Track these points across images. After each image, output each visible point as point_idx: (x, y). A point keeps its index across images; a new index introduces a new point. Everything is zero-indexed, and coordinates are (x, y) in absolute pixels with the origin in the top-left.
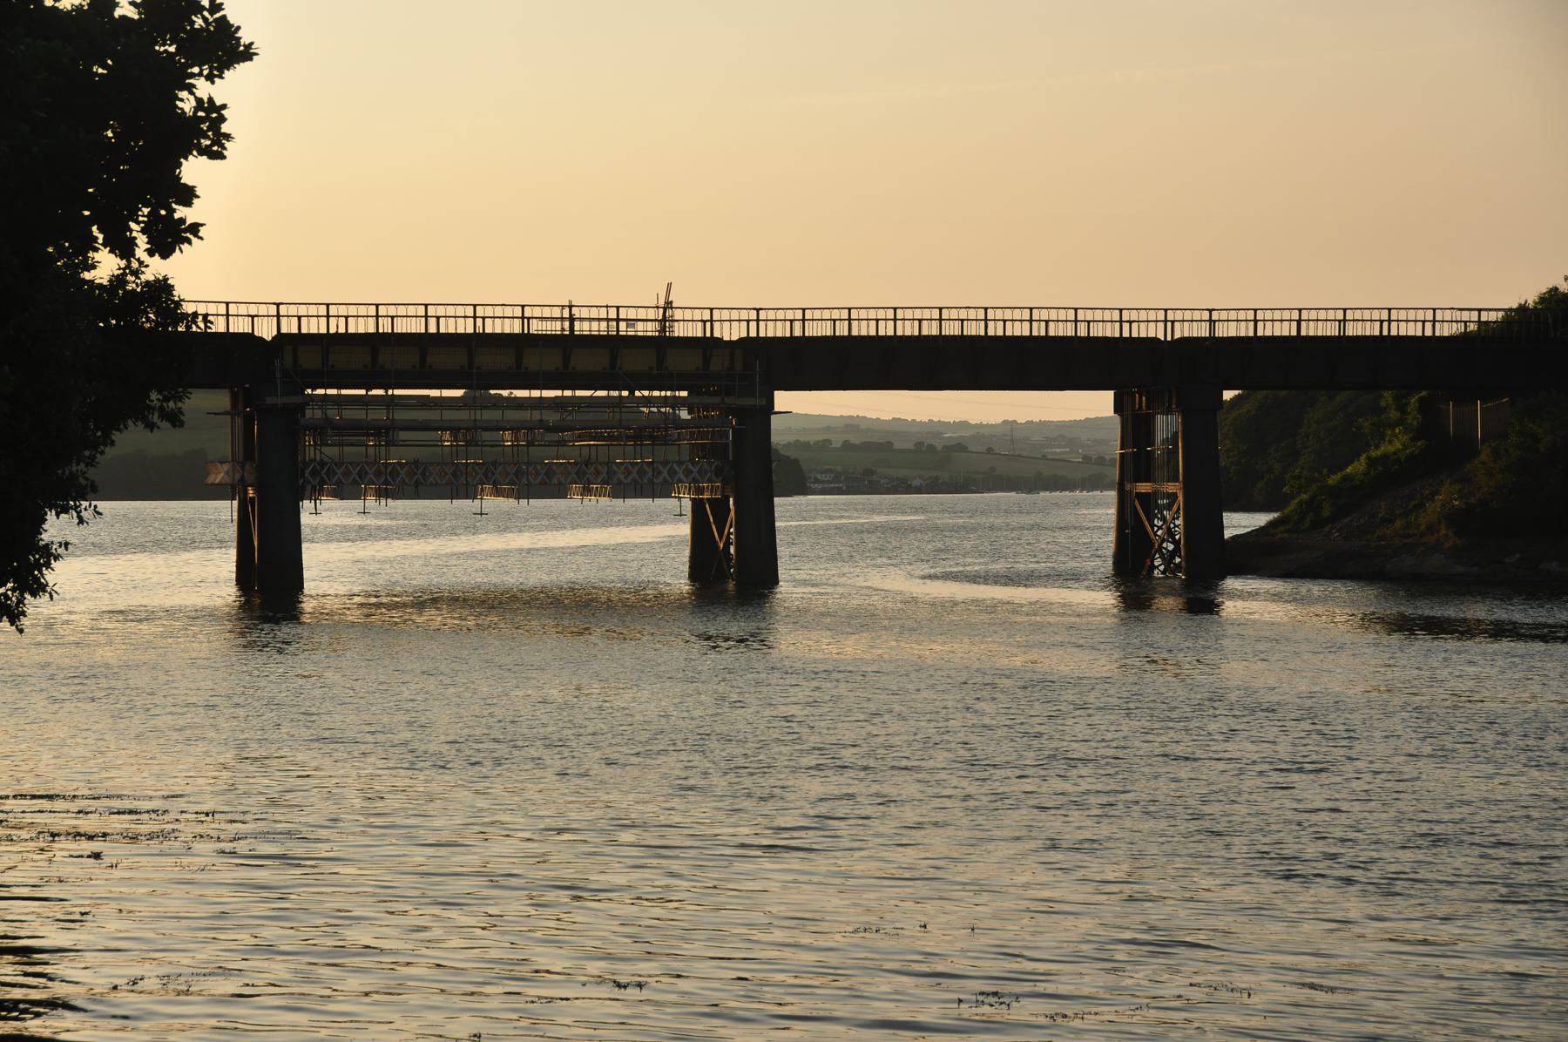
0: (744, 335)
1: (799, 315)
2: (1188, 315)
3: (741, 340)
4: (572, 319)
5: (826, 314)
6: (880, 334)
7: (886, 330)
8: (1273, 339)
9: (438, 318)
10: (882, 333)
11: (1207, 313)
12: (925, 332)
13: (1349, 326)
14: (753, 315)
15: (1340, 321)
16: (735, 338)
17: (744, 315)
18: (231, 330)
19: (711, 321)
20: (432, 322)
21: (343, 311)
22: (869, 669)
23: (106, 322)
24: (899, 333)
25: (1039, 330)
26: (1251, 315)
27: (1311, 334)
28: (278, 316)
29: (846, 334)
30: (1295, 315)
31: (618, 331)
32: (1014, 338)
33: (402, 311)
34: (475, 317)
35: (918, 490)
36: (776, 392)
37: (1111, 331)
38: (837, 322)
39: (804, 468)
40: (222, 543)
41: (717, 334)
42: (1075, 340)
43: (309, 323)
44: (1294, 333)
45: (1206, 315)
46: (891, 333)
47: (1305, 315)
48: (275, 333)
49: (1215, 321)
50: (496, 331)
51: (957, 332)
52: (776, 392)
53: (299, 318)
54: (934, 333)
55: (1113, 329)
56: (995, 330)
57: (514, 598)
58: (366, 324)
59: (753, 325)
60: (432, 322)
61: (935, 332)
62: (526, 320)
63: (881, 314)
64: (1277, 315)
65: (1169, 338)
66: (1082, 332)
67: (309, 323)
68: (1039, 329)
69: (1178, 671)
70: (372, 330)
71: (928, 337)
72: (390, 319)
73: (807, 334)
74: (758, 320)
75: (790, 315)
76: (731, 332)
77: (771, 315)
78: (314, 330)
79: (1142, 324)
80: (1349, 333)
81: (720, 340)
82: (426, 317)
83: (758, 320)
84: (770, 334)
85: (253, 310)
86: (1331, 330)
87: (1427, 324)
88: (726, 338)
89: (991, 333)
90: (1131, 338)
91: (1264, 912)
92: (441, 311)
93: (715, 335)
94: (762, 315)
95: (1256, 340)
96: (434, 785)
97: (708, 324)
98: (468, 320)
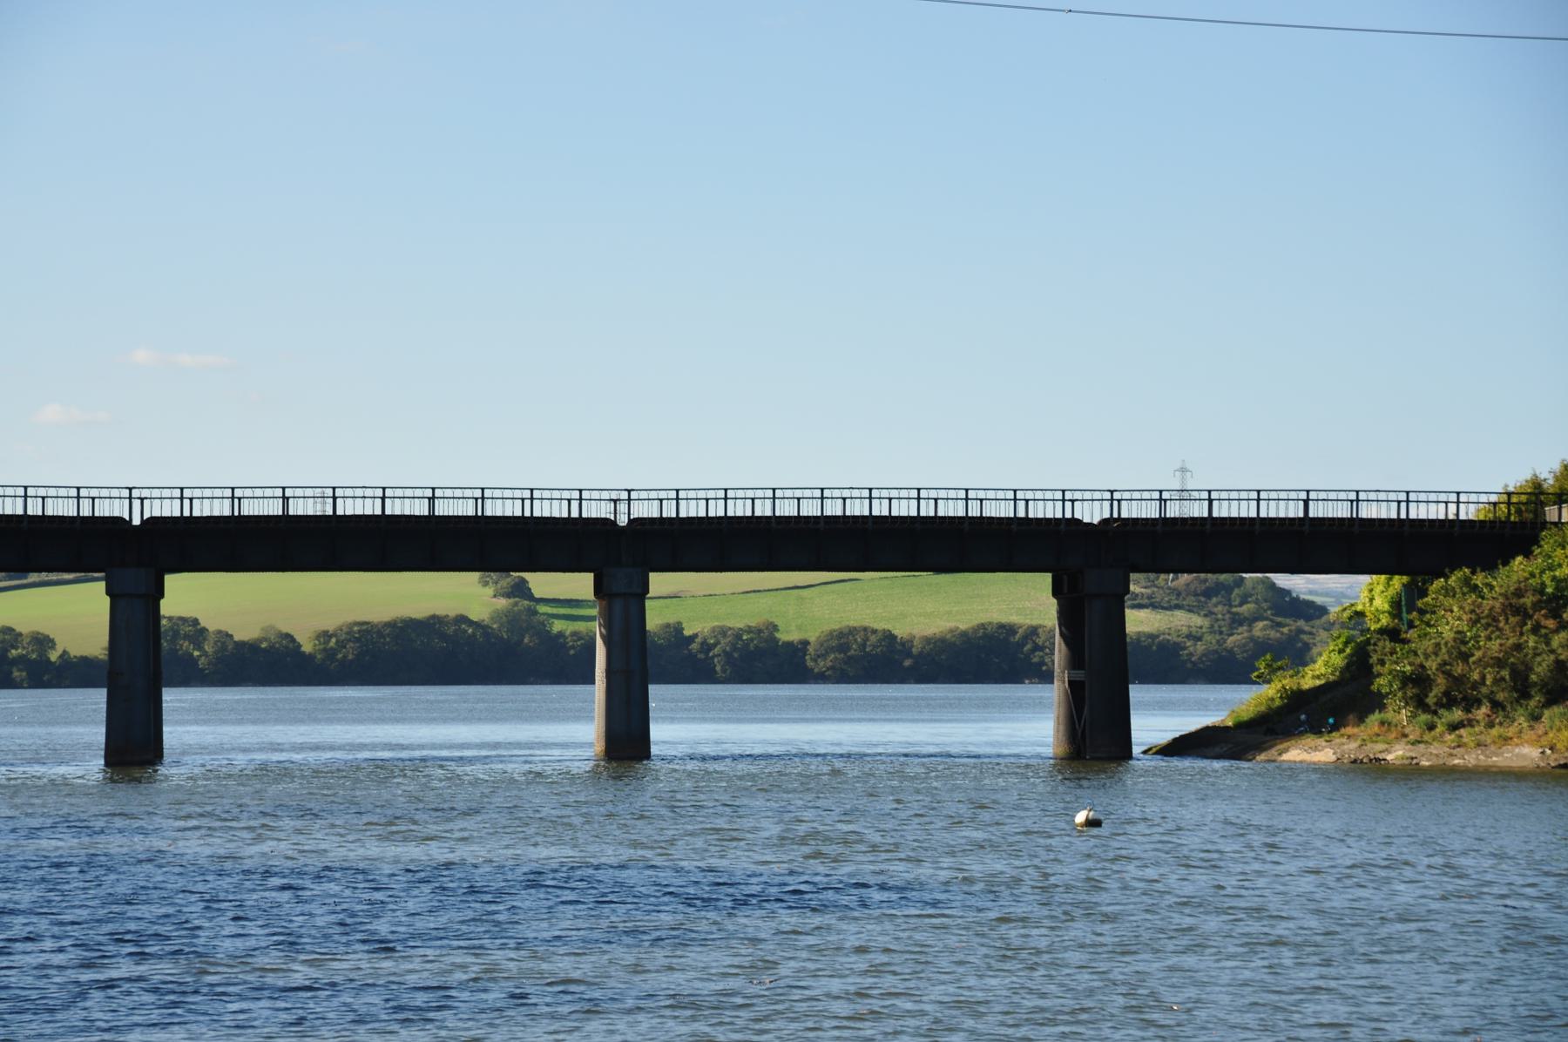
0: (1107, 515)
2: (208, 493)
3: (1104, 522)
5: (653, 495)
6: (874, 513)
7: (717, 510)
8: (1183, 521)
9: (142, 499)
10: (758, 513)
11: (626, 493)
13: (1363, 505)
15: (429, 498)
18: (97, 514)
20: (1021, 505)
21: (933, 494)
22: (1228, 849)
24: (730, 513)
25: (927, 510)
26: (379, 493)
29: (75, 514)
30: (1303, 495)
33: (52, 492)
36: (652, 575)
37: (1003, 510)
38: (96, 500)
40: (94, 722)
42: (78, 520)
44: (1301, 515)
45: (1108, 495)
46: (721, 513)
47: (238, 493)
48: (626, 521)
53: (569, 501)
55: (1201, 508)
56: (880, 509)
59: (575, 504)
60: (1021, 505)
62: (236, 501)
63: (711, 494)
64: (1234, 495)
65: (236, 514)
66: (86, 511)
70: (961, 513)
71: (689, 519)
72: (796, 501)
73: (970, 515)
74: (1408, 501)
76: (1092, 513)
79: (1243, 503)
80: (1364, 514)
81: (1079, 522)
82: (1015, 500)
85: (798, 494)
86: (1295, 511)
87: (1449, 505)
89: (875, 513)
90: (1027, 519)
91: (820, 973)
93: (1076, 516)
95: (1164, 521)
96: (630, 959)
97: (480, 501)
98: (516, 501)
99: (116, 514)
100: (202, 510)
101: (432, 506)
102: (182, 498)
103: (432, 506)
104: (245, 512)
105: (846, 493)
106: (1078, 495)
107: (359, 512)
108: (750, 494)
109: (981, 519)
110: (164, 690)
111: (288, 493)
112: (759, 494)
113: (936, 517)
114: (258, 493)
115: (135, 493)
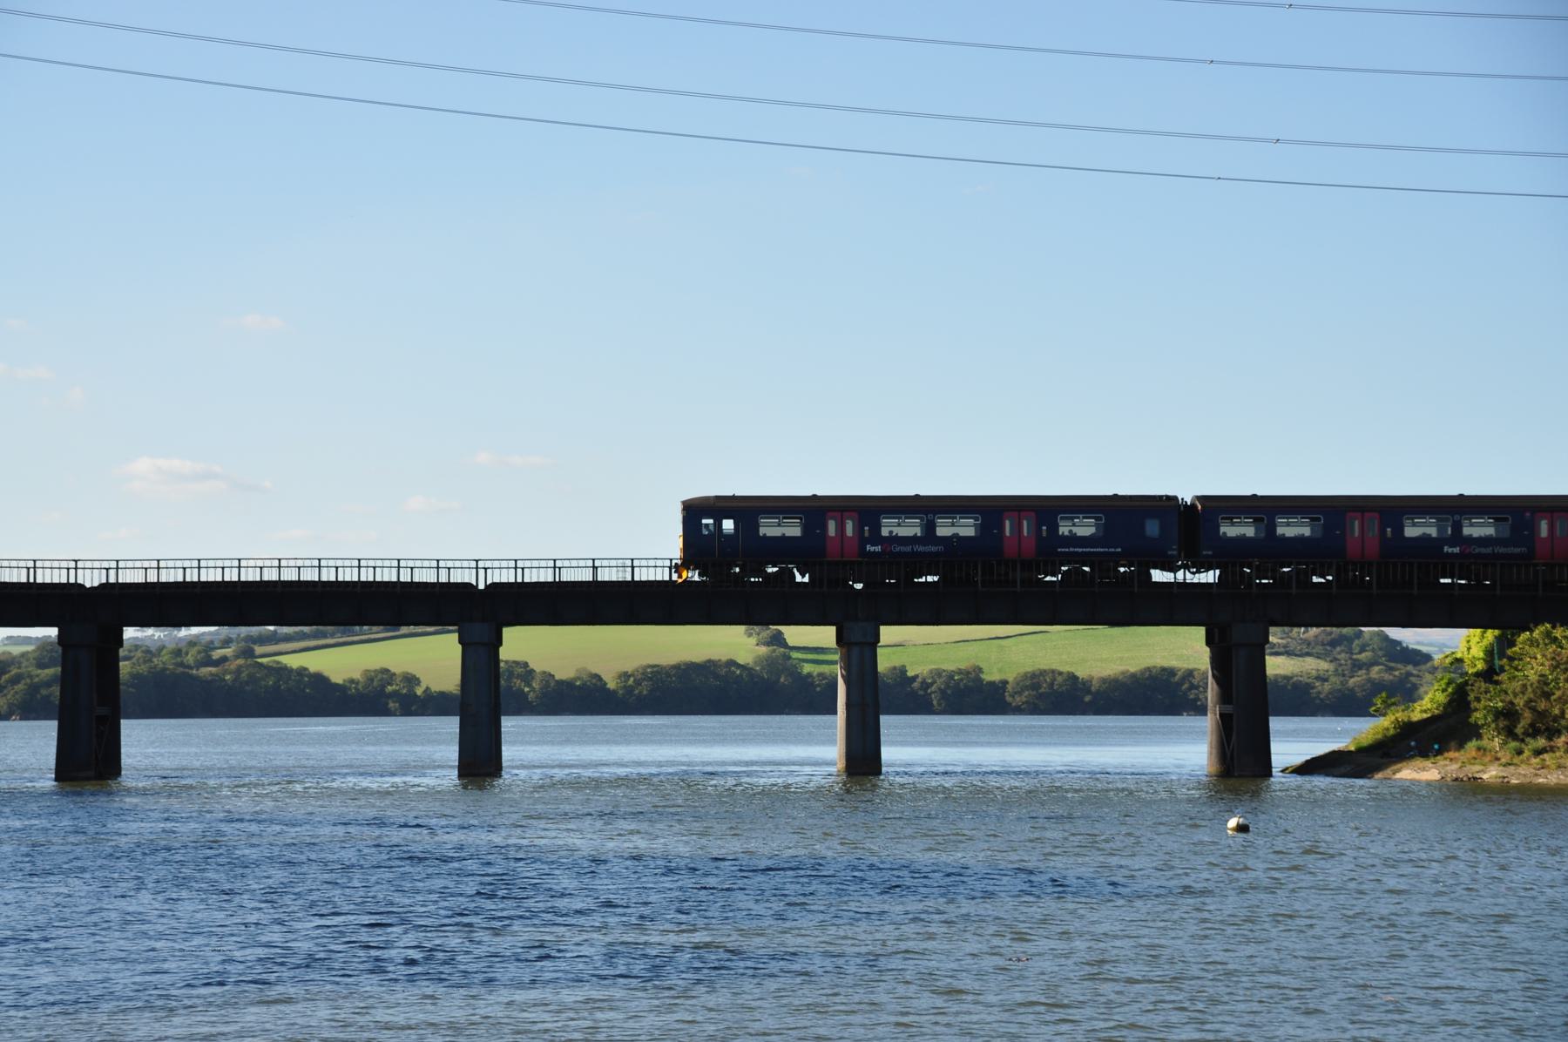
0: (104, 581)
1: (113, 565)
3: (102, 585)
4: (595, 568)
9: (486, 569)
11: (475, 562)
12: (266, 578)
14: (72, 564)
16: (96, 584)
17: (64, 564)
19: (35, 568)
23: (760, 572)
24: (340, 579)
26: (276, 563)
27: (347, 579)
28: (477, 568)
31: (1185, 579)
32: (44, 585)
33: (418, 564)
34: (516, 568)
35: (1018, 711)
36: (834, 628)
39: (121, 676)
41: (80, 581)
43: (531, 573)
45: (473, 564)
47: (559, 564)
49: (597, 568)
50: (46, 581)
51: (295, 578)
52: (834, 628)
54: (274, 579)
57: (757, 762)
58: (176, 574)
59: (72, 572)
61: (235, 579)
62: (557, 570)
65: (557, 580)
67: (531, 573)
68: (192, 574)
69: (668, 864)
70: (219, 579)
73: (282, 579)
74: (76, 568)
75: (106, 565)
76: (90, 579)
77: (644, 563)
78: (348, 579)
79: (210, 570)
83: (76, 568)
84: (48, 580)
85: (300, 563)
87: (70, 570)
88: (88, 585)
92: (488, 564)
94: (80, 564)
97: (32, 571)
98: (354, 569)
99: (467, 581)
100: (568, 576)
101: (595, 574)
102: (516, 568)
103: (595, 574)
104: (564, 579)
105: (339, 563)
106: (528, 564)
107: (652, 578)
108: (260, 563)
109: (449, 585)
110: (503, 718)
111: (597, 563)
112: (227, 563)
113: (223, 581)
114: (574, 563)
115: (481, 564)
